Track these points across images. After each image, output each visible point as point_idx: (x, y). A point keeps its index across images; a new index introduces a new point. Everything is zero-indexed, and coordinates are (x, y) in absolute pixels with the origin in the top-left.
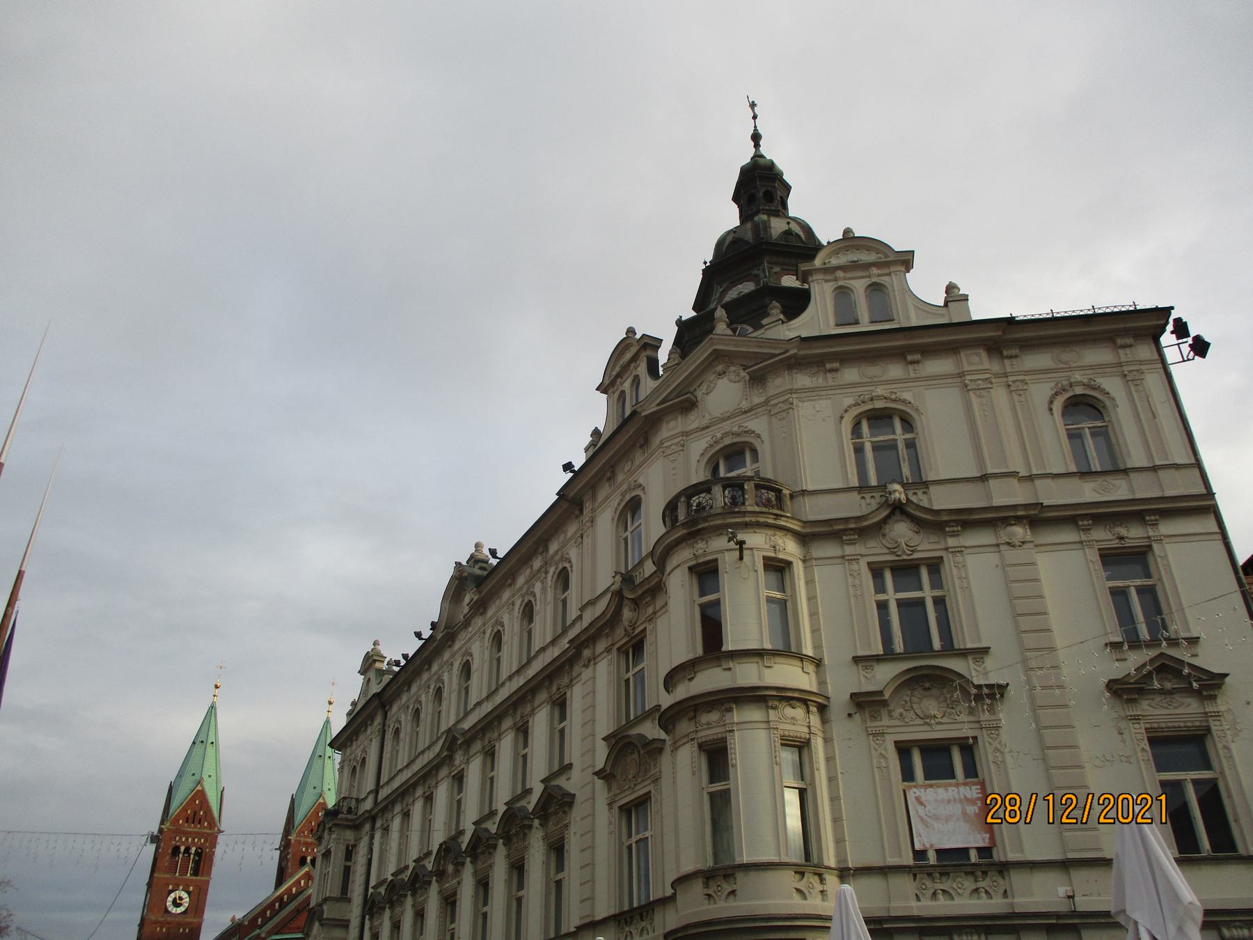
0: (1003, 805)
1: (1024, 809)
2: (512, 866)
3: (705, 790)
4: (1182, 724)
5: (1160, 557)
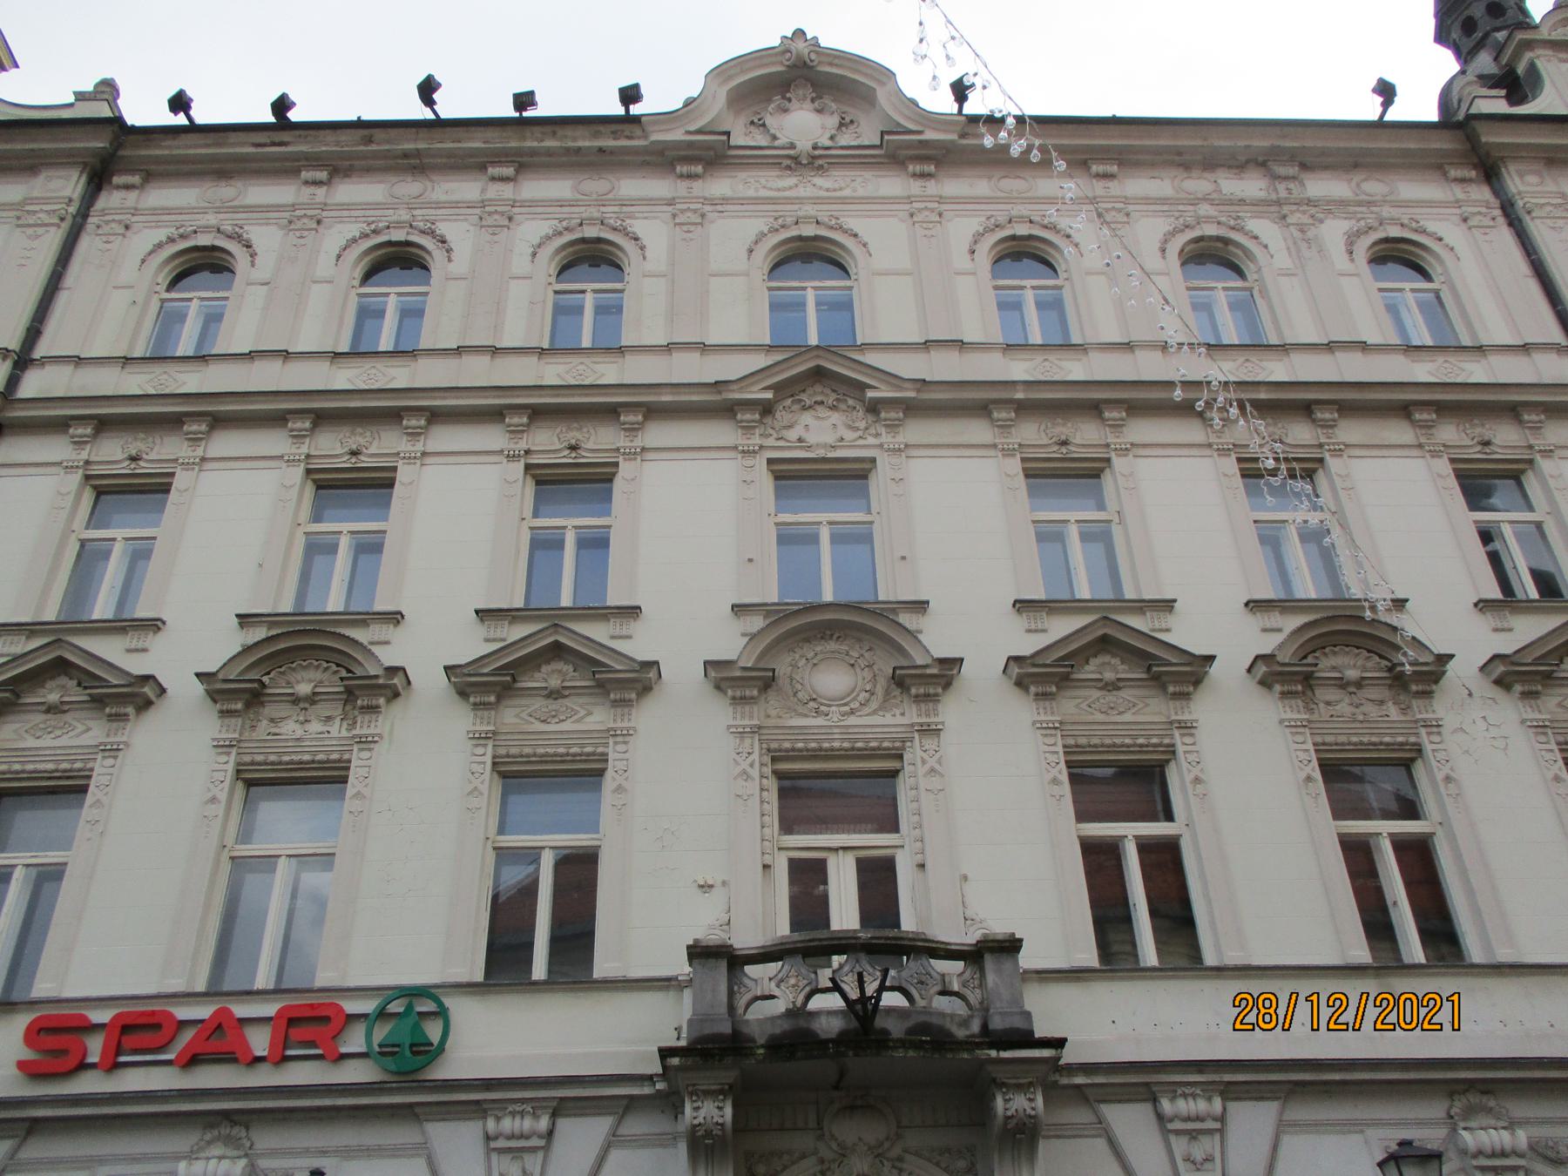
0: (1255, 1008)
1: (1281, 1012)
2: (238, 771)
3: (226, 850)
4: (1127, 741)
5: (1124, 476)
